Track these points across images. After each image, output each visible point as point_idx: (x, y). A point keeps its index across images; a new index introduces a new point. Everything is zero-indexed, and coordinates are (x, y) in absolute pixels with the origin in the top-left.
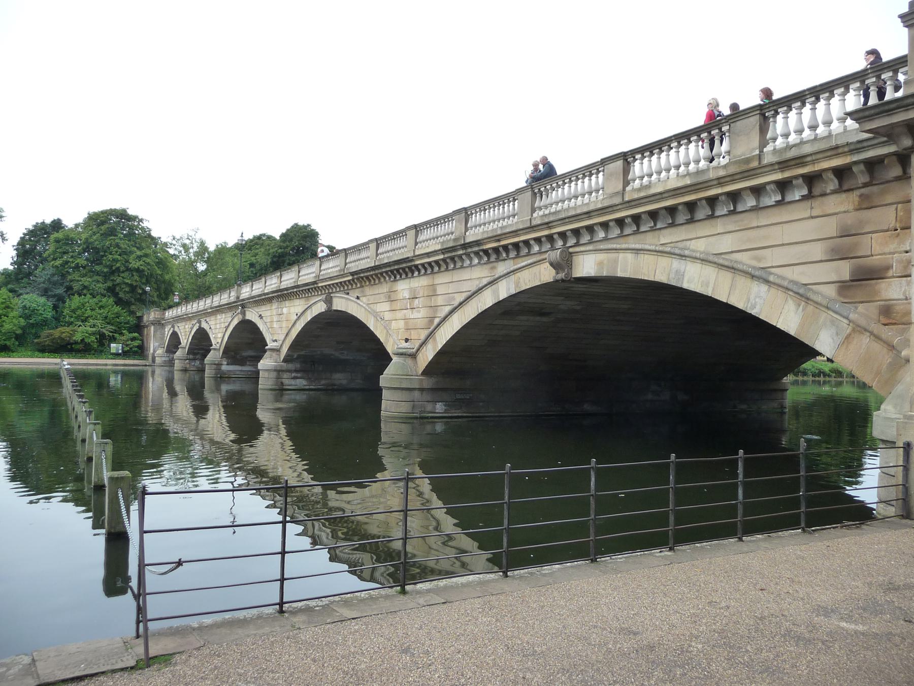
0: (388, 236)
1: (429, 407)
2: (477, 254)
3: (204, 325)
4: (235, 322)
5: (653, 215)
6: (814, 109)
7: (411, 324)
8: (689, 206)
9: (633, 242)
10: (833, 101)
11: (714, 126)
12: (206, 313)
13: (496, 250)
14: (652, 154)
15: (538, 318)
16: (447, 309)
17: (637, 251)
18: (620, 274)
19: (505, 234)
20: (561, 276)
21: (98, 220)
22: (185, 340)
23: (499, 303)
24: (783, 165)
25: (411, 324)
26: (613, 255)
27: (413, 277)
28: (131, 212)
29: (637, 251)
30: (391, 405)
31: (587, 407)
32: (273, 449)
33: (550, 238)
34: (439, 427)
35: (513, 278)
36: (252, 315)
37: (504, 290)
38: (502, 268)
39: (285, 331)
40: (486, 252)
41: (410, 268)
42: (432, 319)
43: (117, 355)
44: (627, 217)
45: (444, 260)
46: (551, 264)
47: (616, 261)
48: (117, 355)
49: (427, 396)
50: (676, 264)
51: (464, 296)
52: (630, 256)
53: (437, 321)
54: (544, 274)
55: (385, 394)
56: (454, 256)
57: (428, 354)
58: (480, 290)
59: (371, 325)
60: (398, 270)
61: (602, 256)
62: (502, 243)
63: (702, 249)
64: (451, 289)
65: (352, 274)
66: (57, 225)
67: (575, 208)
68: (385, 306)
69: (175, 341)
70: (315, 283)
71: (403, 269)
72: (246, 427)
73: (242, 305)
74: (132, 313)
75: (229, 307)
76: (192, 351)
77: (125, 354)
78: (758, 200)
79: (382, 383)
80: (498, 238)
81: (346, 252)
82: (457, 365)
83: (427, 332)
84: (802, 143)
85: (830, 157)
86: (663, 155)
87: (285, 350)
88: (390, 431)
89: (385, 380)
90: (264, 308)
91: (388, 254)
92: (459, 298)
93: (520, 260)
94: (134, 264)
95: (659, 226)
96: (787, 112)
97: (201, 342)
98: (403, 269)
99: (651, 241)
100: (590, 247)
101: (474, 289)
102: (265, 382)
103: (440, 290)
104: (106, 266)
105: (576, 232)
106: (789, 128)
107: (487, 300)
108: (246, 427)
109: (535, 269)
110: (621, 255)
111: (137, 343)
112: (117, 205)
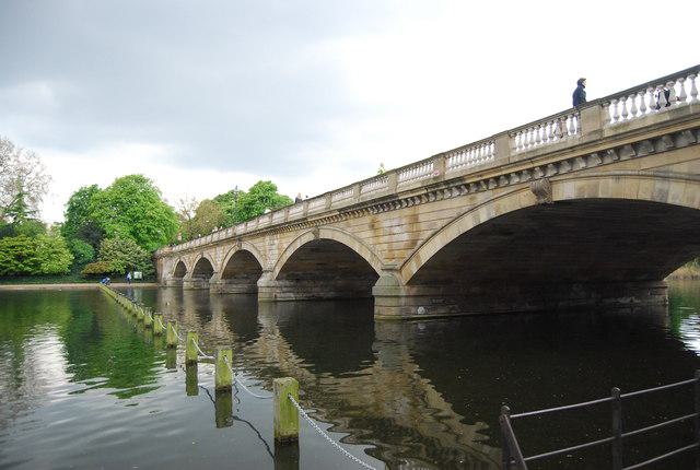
0: (455, 150)
1: (413, 310)
2: (458, 188)
3: (206, 256)
4: (233, 252)
5: (635, 146)
6: (634, 101)
7: (394, 250)
8: (347, 212)
9: (613, 169)
10: (685, 83)
11: (381, 176)
12: (207, 246)
13: (477, 184)
14: (480, 147)
15: (502, 237)
16: (430, 233)
17: (618, 177)
18: (601, 195)
19: (619, 135)
20: (542, 201)
21: (121, 183)
22: (190, 268)
23: (491, 220)
24: (615, 138)
25: (394, 250)
26: (593, 182)
27: (395, 209)
28: (145, 176)
29: (618, 177)
30: (384, 309)
31: (528, 307)
32: (271, 345)
33: (531, 171)
34: (421, 327)
35: (493, 204)
36: (246, 246)
37: (484, 216)
38: (481, 198)
39: (277, 257)
40: (467, 186)
41: (393, 202)
42: (414, 242)
43: (138, 280)
44: (609, 149)
45: (427, 195)
46: (534, 192)
47: (597, 186)
48: (138, 280)
49: (411, 301)
50: (659, 185)
51: (445, 222)
52: (611, 181)
53: (420, 242)
54: (525, 199)
55: (377, 301)
56: (436, 189)
57: (414, 268)
58: (460, 216)
59: (356, 248)
60: (381, 205)
61: (580, 183)
62: (484, 178)
63: (686, 171)
64: (433, 216)
65: (340, 210)
66: (94, 189)
67: (481, 166)
68: (369, 234)
69: (181, 270)
70: (303, 219)
71: (388, 203)
72: (205, 315)
73: (239, 238)
74: (147, 248)
75: (228, 240)
76: (196, 273)
77: (143, 279)
78: (587, 163)
79: (374, 293)
80: (479, 174)
81: (308, 201)
82: (440, 276)
83: (410, 252)
84: (554, 145)
85: (611, 142)
86: (523, 135)
87: (277, 270)
88: (382, 332)
89: (377, 289)
90: (257, 240)
91: (252, 226)
92: (440, 224)
93: (499, 190)
94: (149, 213)
95: (640, 154)
96: (616, 103)
97: (204, 268)
98: (388, 203)
99: (631, 166)
100: (571, 176)
101: (455, 215)
102: (262, 296)
103: (421, 218)
104: (130, 216)
105: (557, 165)
106: (522, 143)
107: (468, 223)
108: (205, 315)
109: (514, 197)
110: (602, 181)
111: (153, 271)
112: (136, 172)
